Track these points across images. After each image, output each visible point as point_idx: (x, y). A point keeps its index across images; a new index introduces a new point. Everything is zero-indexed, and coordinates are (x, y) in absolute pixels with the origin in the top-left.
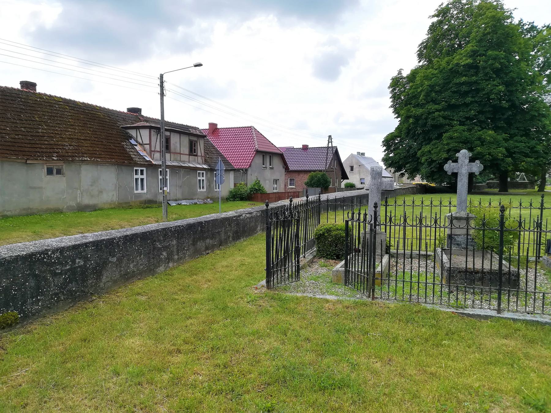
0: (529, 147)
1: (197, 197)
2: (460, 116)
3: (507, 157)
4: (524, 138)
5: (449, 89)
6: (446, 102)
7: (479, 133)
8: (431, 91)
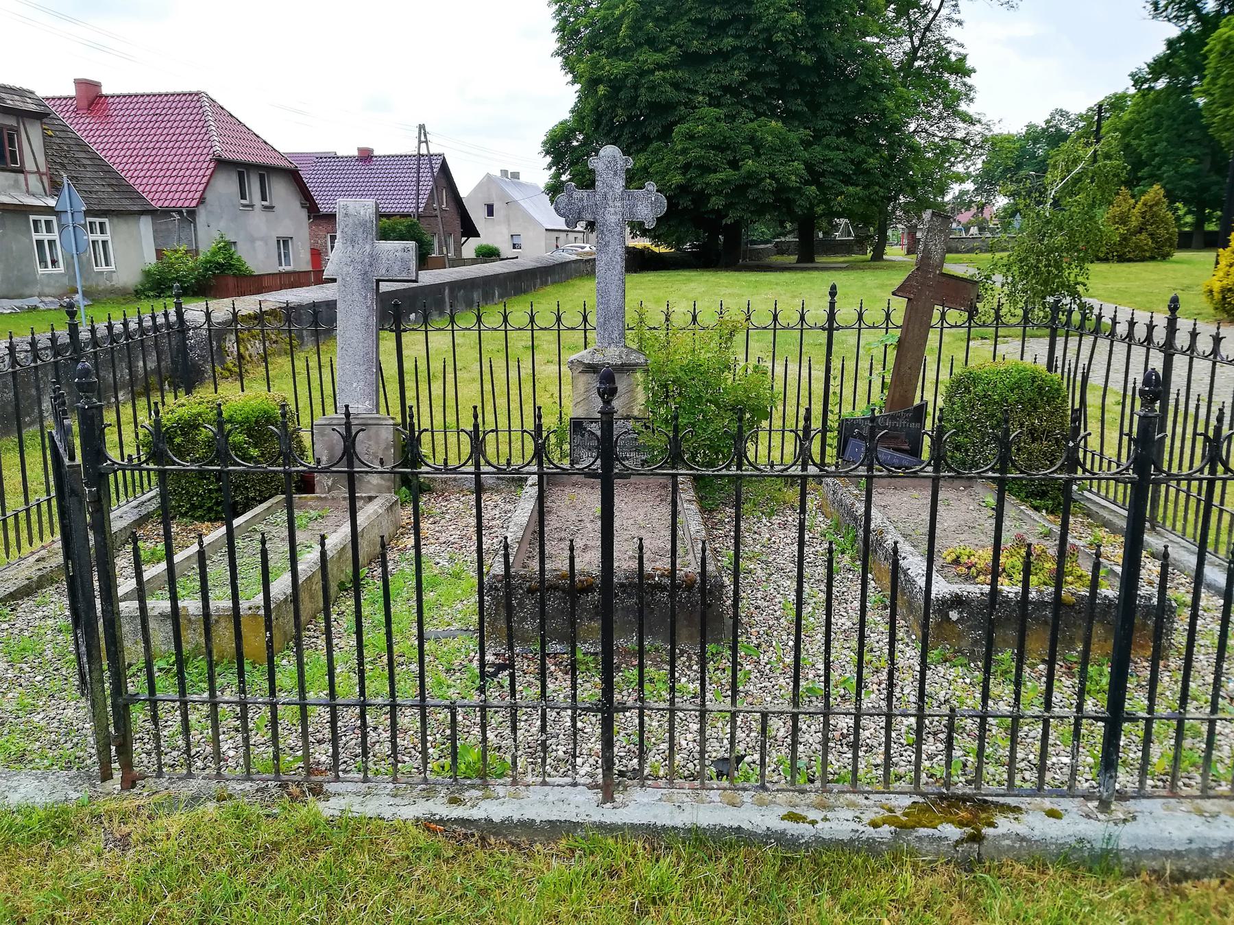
0: (852, 162)
1: (37, 290)
2: (711, 84)
3: (807, 183)
4: (843, 139)
5: (686, 13)
6: (680, 46)
7: (751, 125)
8: (645, 17)
